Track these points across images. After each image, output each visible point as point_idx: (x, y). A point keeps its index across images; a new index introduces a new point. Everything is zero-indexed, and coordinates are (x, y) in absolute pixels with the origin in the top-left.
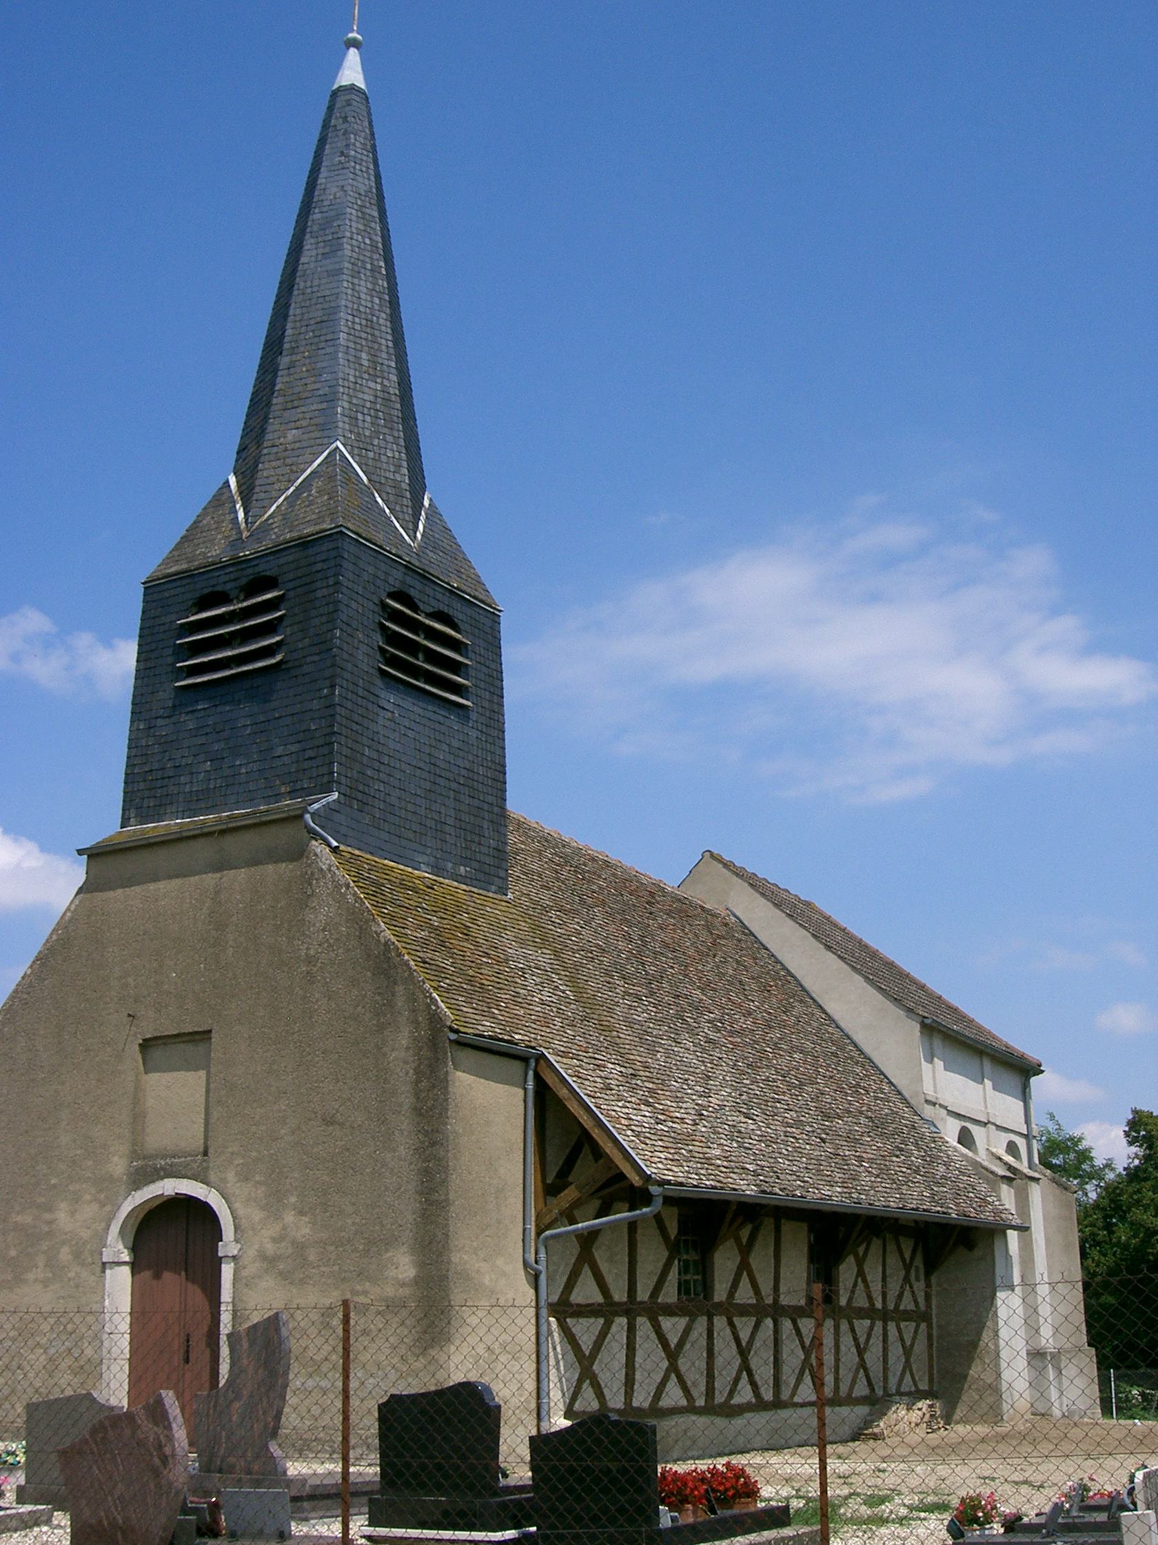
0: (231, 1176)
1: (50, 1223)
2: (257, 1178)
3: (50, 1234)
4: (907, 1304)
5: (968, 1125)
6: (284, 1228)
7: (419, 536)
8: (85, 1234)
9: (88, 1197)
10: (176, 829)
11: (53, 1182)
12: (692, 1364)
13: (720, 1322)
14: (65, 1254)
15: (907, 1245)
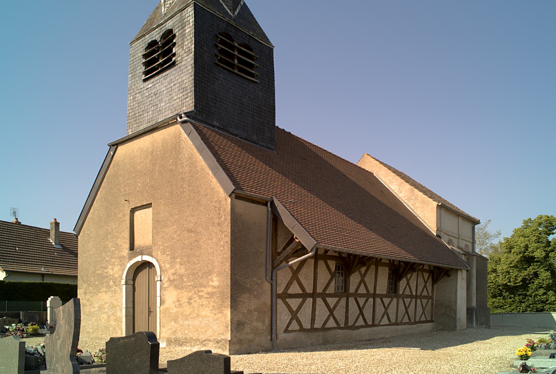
1: (106, 273)
2: (168, 253)
4: (425, 293)
5: (452, 238)
6: (176, 270)
7: (236, 13)
9: (117, 264)
11: (107, 259)
12: (339, 313)
13: (352, 300)
15: (426, 275)
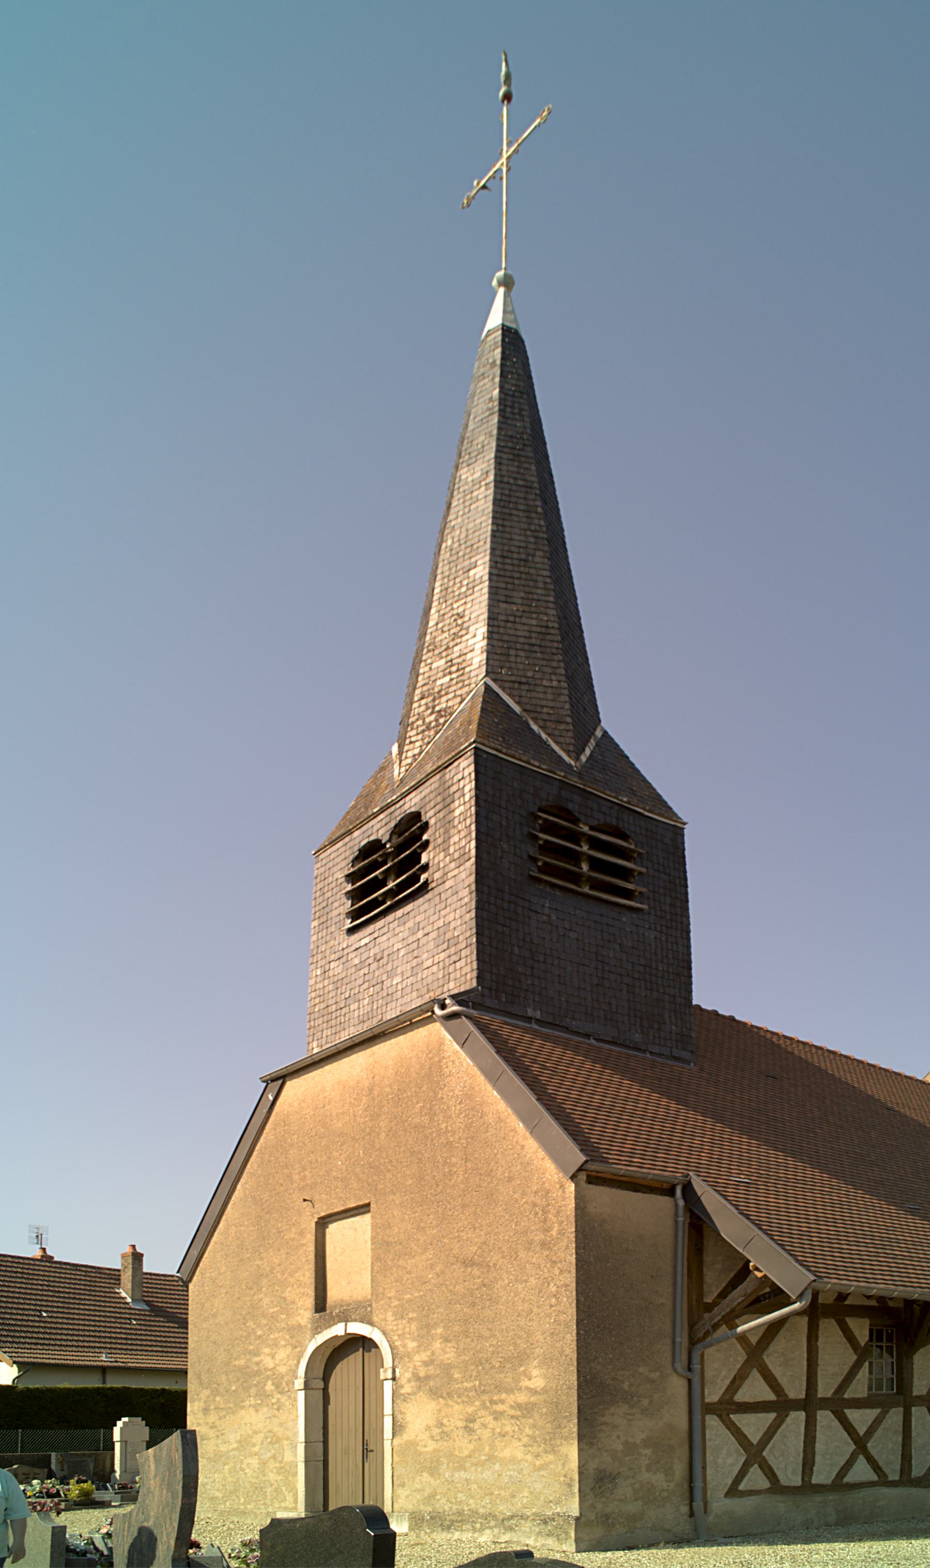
0: (390, 1316)
1: (257, 1364)
2: (411, 1315)
3: (258, 1373)
6: (433, 1354)
8: (283, 1369)
9: (283, 1343)
10: (622, 1172)
14: (269, 1386)
